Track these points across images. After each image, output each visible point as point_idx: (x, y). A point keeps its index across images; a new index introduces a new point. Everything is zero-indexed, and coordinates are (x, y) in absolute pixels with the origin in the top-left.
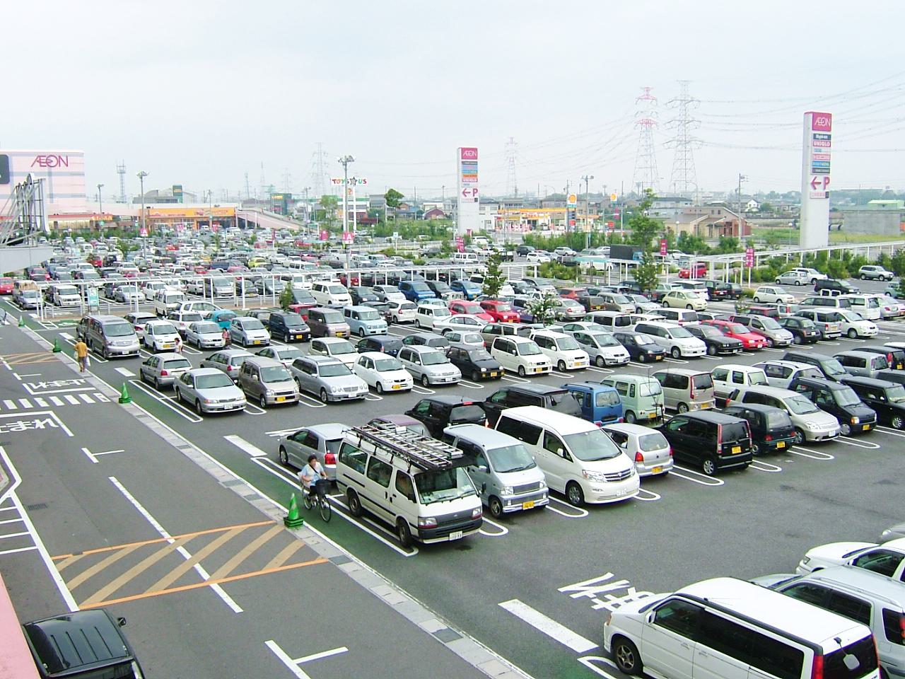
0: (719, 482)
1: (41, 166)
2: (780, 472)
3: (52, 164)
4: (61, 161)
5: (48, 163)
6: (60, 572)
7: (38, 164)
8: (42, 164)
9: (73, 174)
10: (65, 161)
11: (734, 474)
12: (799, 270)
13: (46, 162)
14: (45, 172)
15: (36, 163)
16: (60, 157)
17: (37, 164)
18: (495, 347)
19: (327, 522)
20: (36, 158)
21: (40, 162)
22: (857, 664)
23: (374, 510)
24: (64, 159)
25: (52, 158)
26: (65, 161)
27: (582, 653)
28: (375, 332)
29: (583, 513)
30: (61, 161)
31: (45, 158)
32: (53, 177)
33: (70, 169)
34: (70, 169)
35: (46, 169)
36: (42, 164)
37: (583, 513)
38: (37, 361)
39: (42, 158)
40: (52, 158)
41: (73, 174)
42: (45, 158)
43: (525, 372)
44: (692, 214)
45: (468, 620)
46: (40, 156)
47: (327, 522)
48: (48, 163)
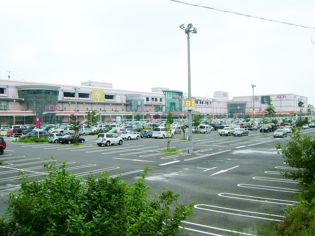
0: (240, 185)
2: (253, 177)
5: (280, 97)
7: (278, 98)
9: (287, 100)
12: (128, 130)
14: (222, 108)
21: (278, 97)
24: (285, 96)
25: (282, 96)
27: (61, 103)
29: (197, 207)
32: (282, 101)
35: (280, 99)
37: (197, 207)
38: (117, 175)
40: (282, 96)
41: (287, 100)
43: (2, 121)
44: (283, 116)
48: (280, 97)
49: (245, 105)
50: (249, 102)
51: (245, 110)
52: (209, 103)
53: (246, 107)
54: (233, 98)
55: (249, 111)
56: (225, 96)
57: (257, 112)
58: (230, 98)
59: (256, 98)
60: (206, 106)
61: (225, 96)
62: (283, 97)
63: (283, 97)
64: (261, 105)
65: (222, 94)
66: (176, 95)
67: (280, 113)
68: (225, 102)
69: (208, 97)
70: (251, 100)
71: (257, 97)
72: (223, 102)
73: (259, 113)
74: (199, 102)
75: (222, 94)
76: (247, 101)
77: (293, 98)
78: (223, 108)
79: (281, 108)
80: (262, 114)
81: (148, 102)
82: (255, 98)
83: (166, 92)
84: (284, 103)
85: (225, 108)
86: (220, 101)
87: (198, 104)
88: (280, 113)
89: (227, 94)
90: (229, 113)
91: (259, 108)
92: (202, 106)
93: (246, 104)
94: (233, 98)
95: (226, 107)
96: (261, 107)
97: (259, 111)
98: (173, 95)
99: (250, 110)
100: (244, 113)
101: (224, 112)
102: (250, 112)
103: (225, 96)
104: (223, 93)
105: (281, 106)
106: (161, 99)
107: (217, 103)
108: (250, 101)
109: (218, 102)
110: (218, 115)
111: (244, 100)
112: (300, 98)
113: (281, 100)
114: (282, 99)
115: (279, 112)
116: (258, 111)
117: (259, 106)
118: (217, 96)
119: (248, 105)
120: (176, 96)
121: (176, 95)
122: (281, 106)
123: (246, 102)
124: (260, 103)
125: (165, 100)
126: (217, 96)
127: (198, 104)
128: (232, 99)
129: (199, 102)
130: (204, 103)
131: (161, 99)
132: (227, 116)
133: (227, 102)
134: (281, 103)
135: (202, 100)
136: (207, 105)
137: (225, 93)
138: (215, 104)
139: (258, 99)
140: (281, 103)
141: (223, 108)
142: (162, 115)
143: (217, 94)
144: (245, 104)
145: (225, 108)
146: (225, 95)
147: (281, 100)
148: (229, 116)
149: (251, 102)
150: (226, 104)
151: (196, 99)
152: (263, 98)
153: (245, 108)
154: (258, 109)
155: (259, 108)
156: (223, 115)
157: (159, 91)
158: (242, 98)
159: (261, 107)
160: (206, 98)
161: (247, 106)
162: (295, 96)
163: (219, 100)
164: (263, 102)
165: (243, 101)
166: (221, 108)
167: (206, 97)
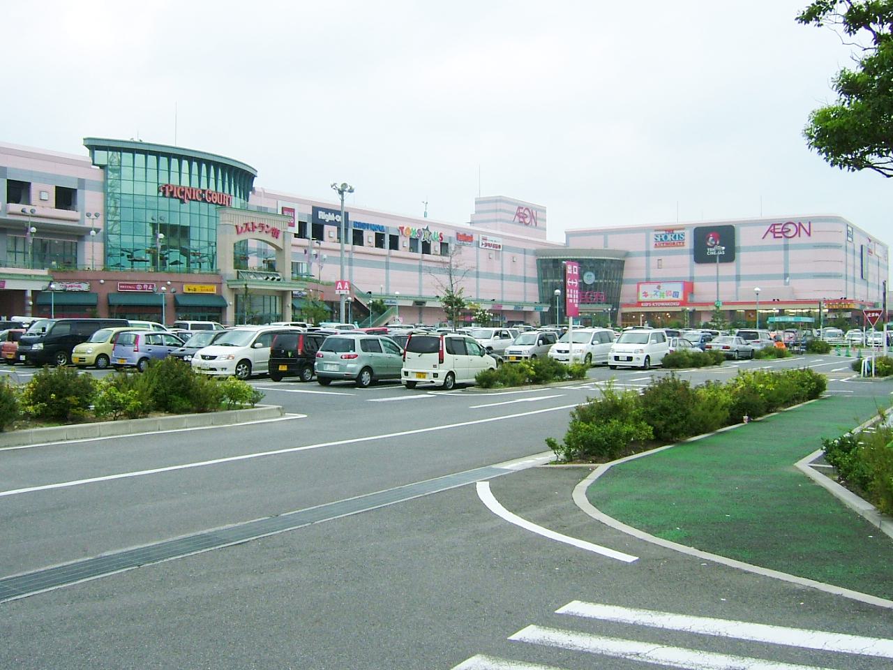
1: (775, 237)
3: (790, 234)
4: (802, 229)
5: (784, 232)
6: (5, 168)
8: (777, 235)
10: (807, 229)
11: (55, 338)
13: (782, 232)
15: (769, 233)
16: (800, 224)
17: (770, 235)
18: (449, 352)
19: (41, 192)
20: (769, 226)
22: (24, 359)
23: (568, 469)
24: (806, 226)
25: (790, 226)
26: (807, 229)
28: (607, 363)
30: (802, 229)
31: (781, 227)
32: (790, 251)
33: (814, 239)
34: (814, 239)
35: (781, 242)
36: (777, 235)
39: (776, 227)
40: (790, 226)
42: (781, 227)
45: (576, 555)
46: (774, 225)
47: (41, 192)
48: (784, 232)
49: (622, 269)
50: (639, 254)
51: (619, 289)
52: (435, 247)
53: (624, 277)
54: (569, 235)
55: (638, 296)
56: (527, 220)
57: (676, 299)
58: (555, 236)
59: (669, 237)
60: (417, 263)
61: (527, 220)
62: (798, 231)
63: (798, 231)
64: (692, 271)
65: (512, 213)
66: (220, 183)
67: (782, 307)
68: (525, 252)
69: (430, 218)
70: (648, 244)
71: (675, 232)
72: (516, 250)
73: (683, 303)
74: (369, 236)
75: (512, 213)
76: (631, 251)
77: (841, 239)
78: (513, 278)
79: (788, 284)
80: (698, 309)
81: (15, 207)
82: (667, 237)
83: (140, 152)
84: (802, 258)
85: (525, 279)
86: (500, 242)
87: (361, 244)
88: (782, 307)
89: (539, 215)
90: (543, 300)
91: (685, 283)
92: (391, 260)
93: (623, 262)
94: (569, 235)
95: (533, 273)
96: (692, 278)
97: (681, 297)
98: (204, 180)
99: (641, 294)
100: (616, 305)
101: (520, 299)
102: (642, 298)
103: (527, 224)
104: (515, 209)
105: (786, 276)
106: (65, 197)
107: (483, 254)
108: (644, 249)
109: (486, 245)
110: (504, 308)
111: (618, 244)
112: (865, 242)
113: (786, 248)
114: (790, 241)
115: (778, 302)
116: (676, 294)
117: (685, 274)
118: (489, 221)
119: (636, 268)
120: (210, 183)
121: (220, 183)
122: (786, 276)
123: (627, 254)
124: (688, 258)
125: (106, 201)
126: (489, 221)
127: (361, 244)
128: (565, 242)
129: (369, 236)
130: (404, 242)
131: (65, 197)
132: (537, 315)
133: (536, 253)
134: (786, 262)
135: (392, 227)
136: (419, 255)
137: (527, 209)
138: (466, 257)
139: (679, 241)
140: (786, 262)
141: (513, 278)
142: (39, 286)
143: (488, 206)
144: (619, 265)
145: (525, 279)
146: (527, 216)
147: (786, 248)
148: (543, 314)
149: (648, 254)
150: (531, 260)
151: (351, 218)
152: (702, 234)
153: (621, 281)
154: (678, 288)
155: (685, 283)
156: (511, 308)
157: (256, 209)
158: (609, 237)
159: (692, 278)
160: (425, 222)
161: (627, 275)
162: (850, 229)
163: (491, 240)
164: (701, 256)
165: (610, 247)
166: (502, 277)
167: (421, 217)
